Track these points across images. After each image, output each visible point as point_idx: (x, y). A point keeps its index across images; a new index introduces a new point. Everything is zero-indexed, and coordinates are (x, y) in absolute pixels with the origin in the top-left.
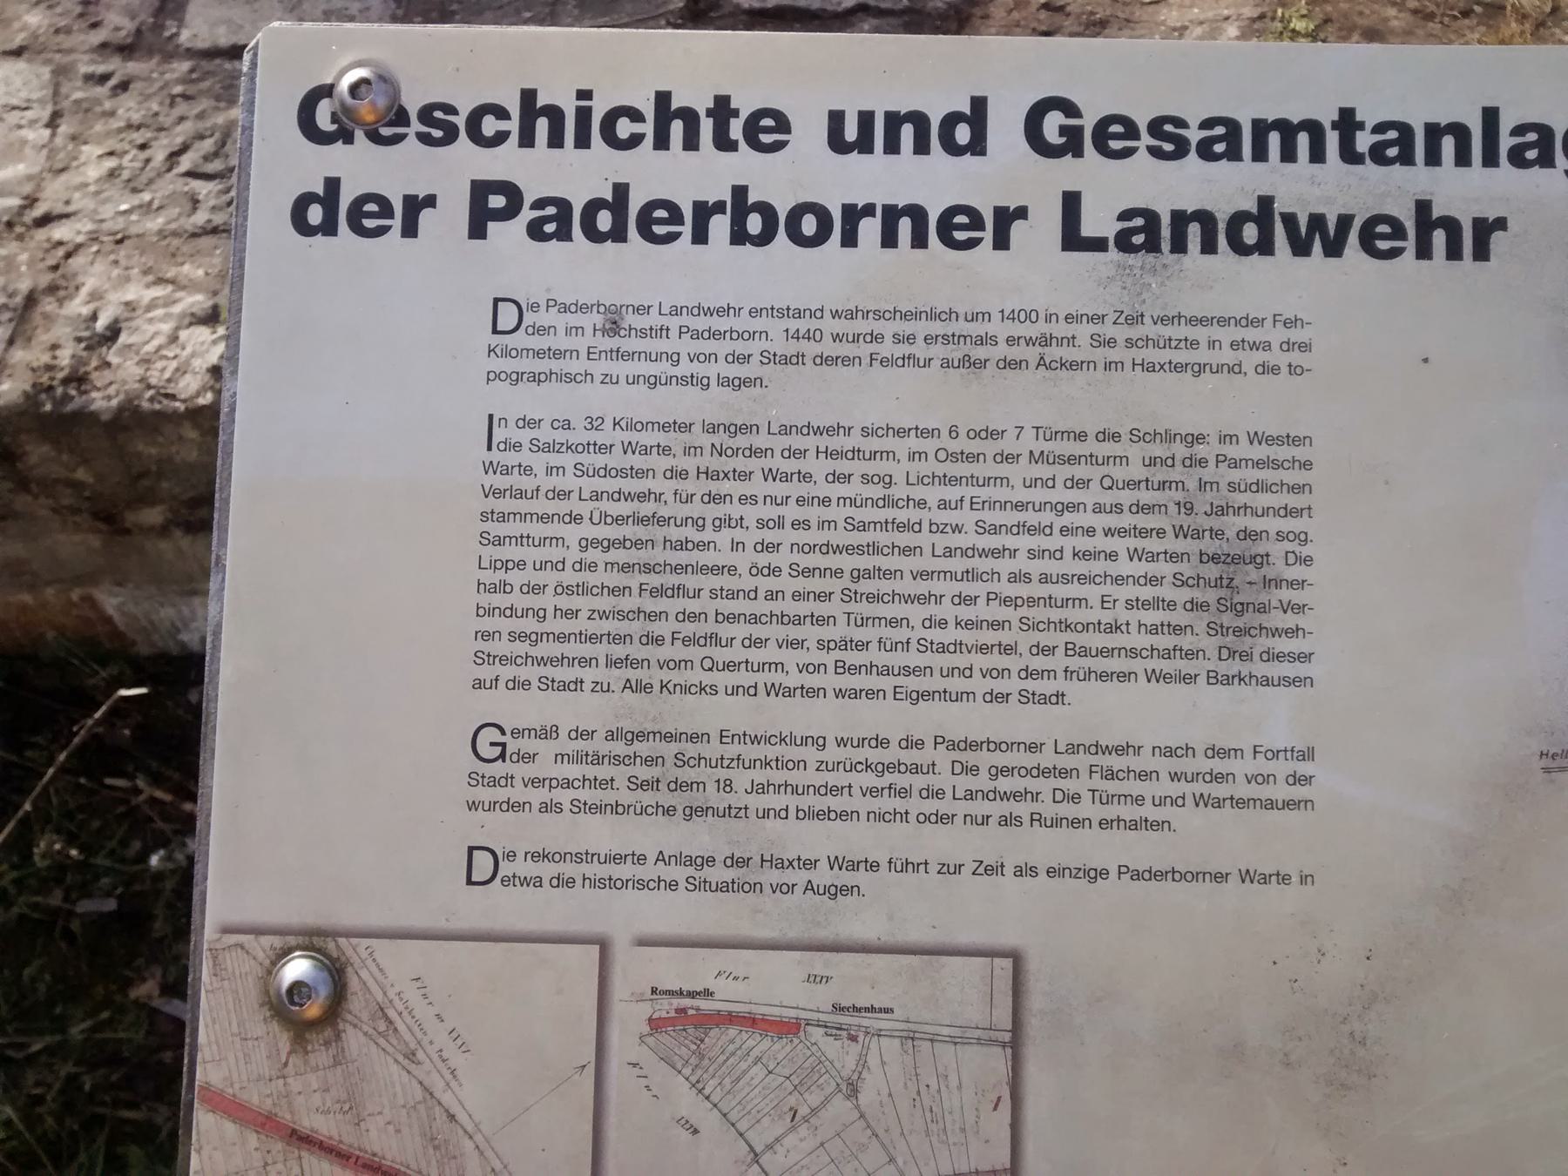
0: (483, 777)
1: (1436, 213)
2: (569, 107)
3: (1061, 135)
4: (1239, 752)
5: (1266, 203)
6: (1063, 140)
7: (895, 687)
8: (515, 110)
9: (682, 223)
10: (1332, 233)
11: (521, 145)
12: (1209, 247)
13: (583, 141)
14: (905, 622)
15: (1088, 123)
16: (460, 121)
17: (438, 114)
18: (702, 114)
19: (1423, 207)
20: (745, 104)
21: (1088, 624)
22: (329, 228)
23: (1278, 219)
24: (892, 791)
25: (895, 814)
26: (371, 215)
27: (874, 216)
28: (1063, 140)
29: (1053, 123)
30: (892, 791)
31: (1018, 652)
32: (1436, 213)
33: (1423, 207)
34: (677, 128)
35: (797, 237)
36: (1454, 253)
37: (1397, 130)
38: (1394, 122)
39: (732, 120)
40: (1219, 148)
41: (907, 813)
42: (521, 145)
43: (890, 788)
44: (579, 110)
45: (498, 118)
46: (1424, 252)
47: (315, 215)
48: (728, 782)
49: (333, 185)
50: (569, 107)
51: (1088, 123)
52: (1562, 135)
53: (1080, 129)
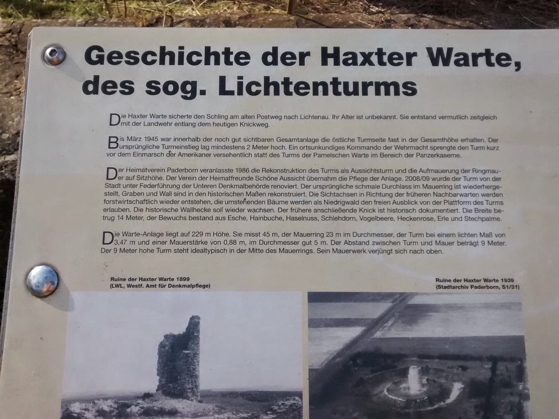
1: (271, 80)
2: (176, 52)
3: (97, 57)
4: (349, 235)
6: (98, 59)
7: (438, 216)
8: (203, 53)
9: (309, 89)
11: (205, 64)
13: (181, 62)
14: (209, 202)
15: (106, 54)
16: (140, 57)
17: (132, 55)
18: (221, 54)
19: (267, 79)
20: (235, 50)
21: (427, 202)
22: (95, 92)
25: (224, 250)
27: (373, 85)
28: (98, 59)
29: (94, 55)
32: (271, 80)
34: (212, 58)
35: (167, 92)
37: (463, 55)
38: (462, 53)
39: (231, 55)
40: (462, 62)
41: (188, 249)
42: (205, 64)
44: (179, 53)
45: (152, 55)
48: (235, 241)
49: (97, 78)
50: (176, 52)
51: (106, 54)
52: (280, 56)
53: (103, 56)
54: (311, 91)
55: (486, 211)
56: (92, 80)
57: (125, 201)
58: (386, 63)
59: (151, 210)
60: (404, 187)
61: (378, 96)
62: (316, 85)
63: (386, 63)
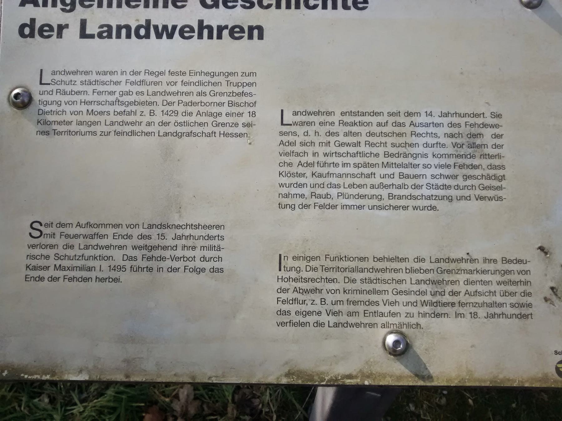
0: (433, 185)
5: (148, 22)
10: (165, 32)
12: (128, 36)
19: (201, 22)
22: (32, 35)
23: (229, 29)
24: (291, 323)
26: (46, 31)
30: (291, 323)
31: (120, 281)
33: (201, 22)
36: (210, 37)
43: (290, 322)
46: (200, 36)
47: (27, 31)
49: (33, 21)
54: (246, 35)
55: (509, 282)
56: (29, 23)
57: (333, 153)
58: (350, 7)
59: (424, 156)
60: (496, 167)
61: (128, 39)
62: (251, 29)
63: (350, 7)
